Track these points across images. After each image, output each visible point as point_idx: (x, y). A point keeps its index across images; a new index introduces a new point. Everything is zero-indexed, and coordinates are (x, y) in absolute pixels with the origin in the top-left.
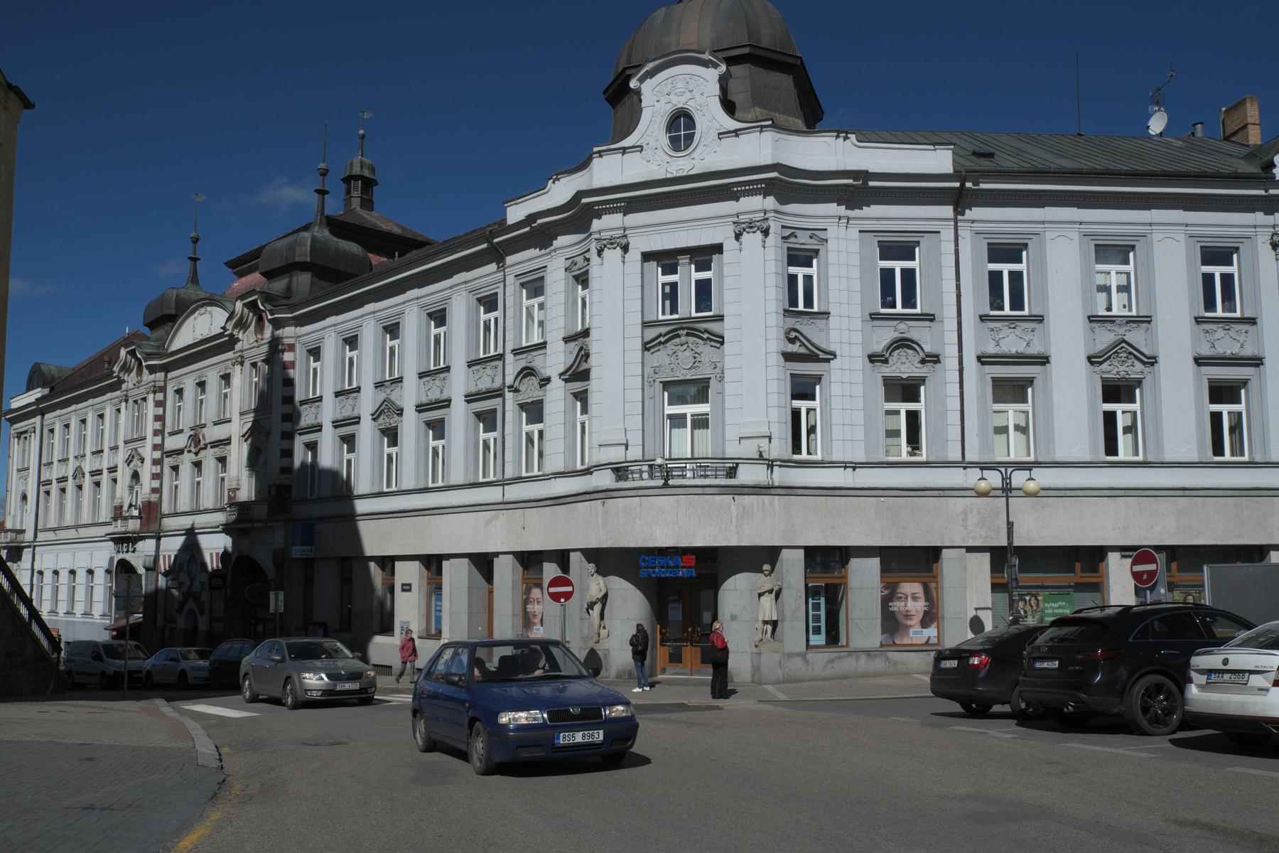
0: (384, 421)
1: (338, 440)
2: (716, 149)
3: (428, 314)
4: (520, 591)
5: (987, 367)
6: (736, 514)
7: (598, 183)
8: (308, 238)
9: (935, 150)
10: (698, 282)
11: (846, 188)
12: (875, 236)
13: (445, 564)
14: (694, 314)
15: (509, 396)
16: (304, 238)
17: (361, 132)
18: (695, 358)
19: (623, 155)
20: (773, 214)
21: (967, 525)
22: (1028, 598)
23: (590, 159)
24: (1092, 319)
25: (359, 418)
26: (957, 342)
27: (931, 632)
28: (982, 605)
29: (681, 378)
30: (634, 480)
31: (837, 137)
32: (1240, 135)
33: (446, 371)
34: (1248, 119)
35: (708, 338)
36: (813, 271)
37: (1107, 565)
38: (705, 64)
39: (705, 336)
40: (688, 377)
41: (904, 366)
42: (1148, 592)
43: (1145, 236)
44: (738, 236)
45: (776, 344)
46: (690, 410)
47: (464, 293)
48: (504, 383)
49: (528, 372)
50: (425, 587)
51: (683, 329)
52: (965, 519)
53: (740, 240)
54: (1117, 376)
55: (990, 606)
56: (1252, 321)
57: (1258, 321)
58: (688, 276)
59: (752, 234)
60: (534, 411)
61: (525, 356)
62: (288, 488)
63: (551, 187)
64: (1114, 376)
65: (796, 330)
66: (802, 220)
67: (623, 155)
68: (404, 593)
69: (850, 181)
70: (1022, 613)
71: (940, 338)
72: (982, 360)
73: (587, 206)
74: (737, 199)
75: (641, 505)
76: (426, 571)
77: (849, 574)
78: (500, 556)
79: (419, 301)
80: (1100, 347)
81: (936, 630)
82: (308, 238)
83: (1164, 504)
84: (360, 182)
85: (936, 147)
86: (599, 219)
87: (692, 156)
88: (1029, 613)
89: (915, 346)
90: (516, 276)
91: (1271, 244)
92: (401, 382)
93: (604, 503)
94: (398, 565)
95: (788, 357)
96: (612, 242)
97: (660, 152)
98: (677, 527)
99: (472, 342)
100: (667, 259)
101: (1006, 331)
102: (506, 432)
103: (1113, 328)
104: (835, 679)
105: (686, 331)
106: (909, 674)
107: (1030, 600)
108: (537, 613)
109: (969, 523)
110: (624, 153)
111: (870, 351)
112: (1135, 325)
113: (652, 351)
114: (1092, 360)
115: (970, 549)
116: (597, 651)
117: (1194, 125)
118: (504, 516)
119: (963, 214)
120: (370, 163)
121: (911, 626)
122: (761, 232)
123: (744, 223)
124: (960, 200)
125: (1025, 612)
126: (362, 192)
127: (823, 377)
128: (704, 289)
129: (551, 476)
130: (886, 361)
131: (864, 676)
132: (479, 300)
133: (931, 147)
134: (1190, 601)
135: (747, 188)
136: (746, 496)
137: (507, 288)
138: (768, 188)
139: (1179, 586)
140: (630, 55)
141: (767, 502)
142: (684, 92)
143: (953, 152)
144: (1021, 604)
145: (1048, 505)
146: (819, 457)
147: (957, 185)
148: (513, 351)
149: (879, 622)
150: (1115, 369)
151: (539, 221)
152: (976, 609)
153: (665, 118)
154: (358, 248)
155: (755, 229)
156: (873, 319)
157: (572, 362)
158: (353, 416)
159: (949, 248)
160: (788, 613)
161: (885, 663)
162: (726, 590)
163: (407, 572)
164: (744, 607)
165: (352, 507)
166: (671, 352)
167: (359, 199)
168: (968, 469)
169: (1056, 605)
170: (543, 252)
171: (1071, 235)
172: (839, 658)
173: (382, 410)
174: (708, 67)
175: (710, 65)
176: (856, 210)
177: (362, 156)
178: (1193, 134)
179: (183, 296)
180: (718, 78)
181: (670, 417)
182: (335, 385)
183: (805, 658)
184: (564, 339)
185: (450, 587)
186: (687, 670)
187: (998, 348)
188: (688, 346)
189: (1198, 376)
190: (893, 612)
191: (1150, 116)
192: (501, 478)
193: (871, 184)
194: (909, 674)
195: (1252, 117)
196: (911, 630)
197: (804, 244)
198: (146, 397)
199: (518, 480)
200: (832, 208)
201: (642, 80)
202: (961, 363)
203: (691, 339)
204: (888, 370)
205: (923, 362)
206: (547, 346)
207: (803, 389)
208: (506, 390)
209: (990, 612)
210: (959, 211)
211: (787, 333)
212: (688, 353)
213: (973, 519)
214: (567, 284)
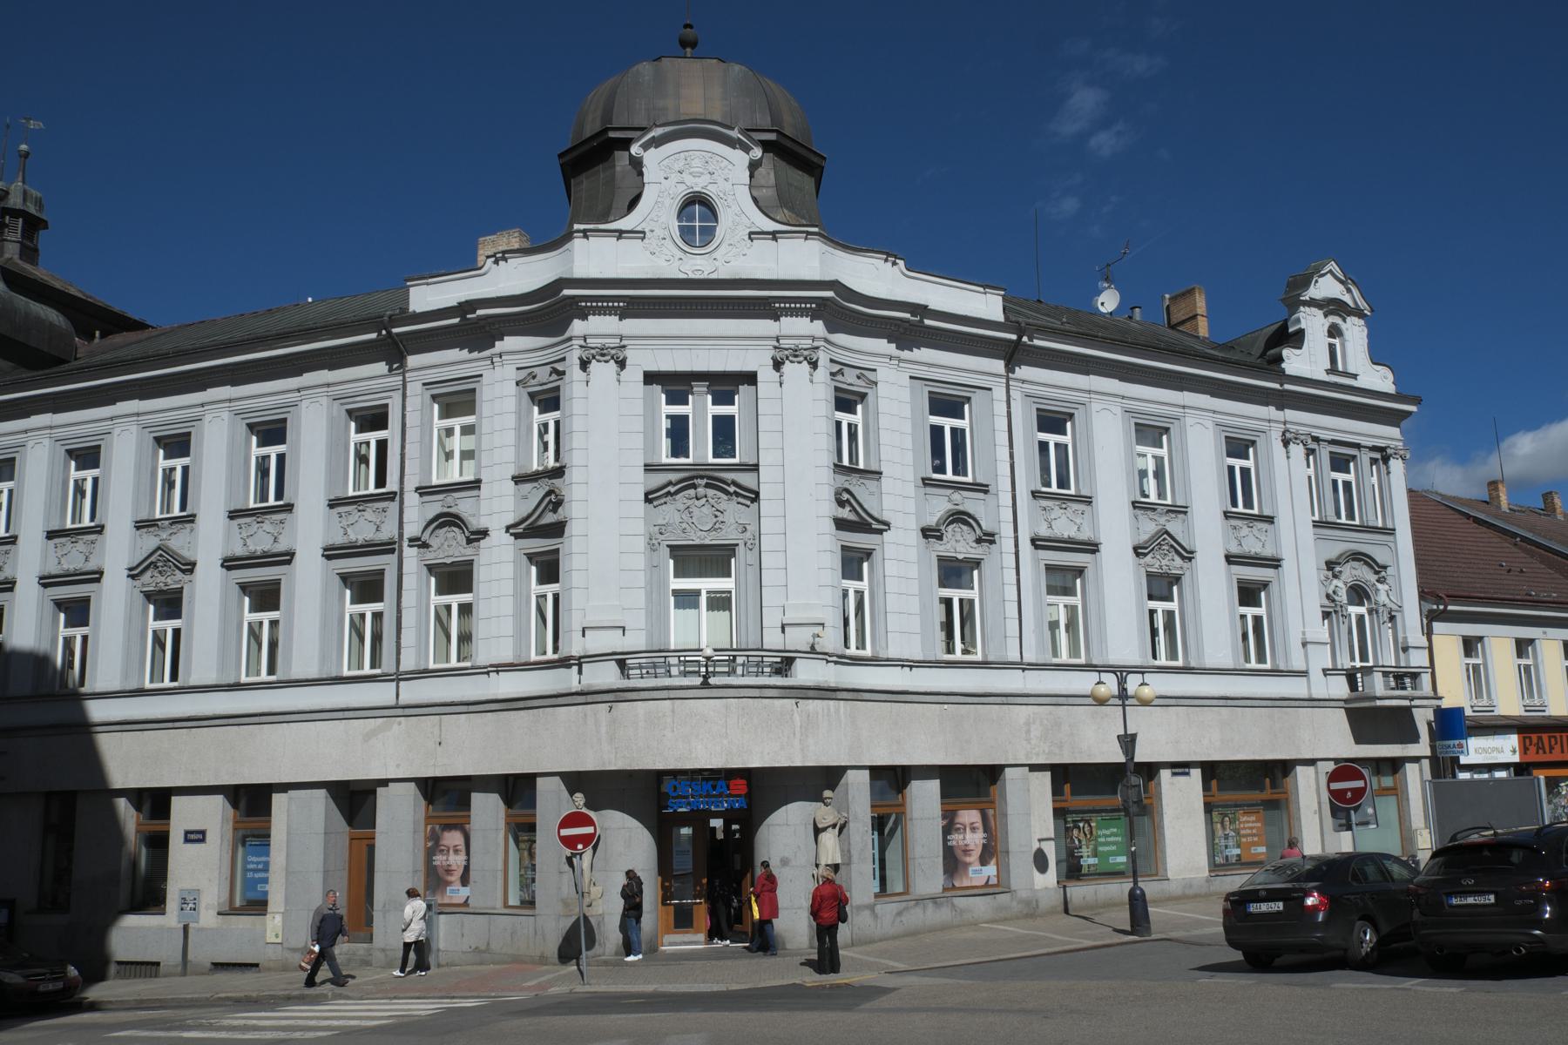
0: (151, 580)
1: (50, 606)
2: (746, 251)
3: (248, 425)
4: (423, 834)
5: (1040, 552)
6: (799, 724)
7: (580, 272)
9: (985, 293)
10: (716, 418)
11: (899, 322)
12: (926, 385)
13: (278, 800)
14: (711, 460)
15: (410, 553)
17: (24, 147)
18: (716, 517)
19: (618, 239)
20: (823, 343)
21: (1031, 739)
22: (1081, 825)
23: (568, 237)
24: (1137, 505)
25: (101, 573)
26: (1012, 520)
27: (991, 870)
28: (1045, 836)
29: (697, 542)
30: (656, 677)
31: (886, 260)
32: (1188, 325)
33: (288, 510)
34: (1198, 310)
35: (735, 492)
36: (857, 418)
37: (1159, 784)
38: (731, 143)
39: (732, 489)
40: (707, 542)
41: (959, 544)
42: (1352, 812)
43: (110, 433)
44: (777, 365)
45: (829, 509)
46: (705, 585)
47: (324, 401)
48: (401, 535)
49: (449, 520)
50: (229, 835)
51: (702, 477)
52: (1028, 732)
53: (588, 370)
54: (1160, 571)
55: (1053, 836)
56: (1270, 520)
57: (1275, 520)
58: (702, 410)
59: (603, 363)
60: (456, 578)
61: (440, 497)
63: (490, 269)
64: (1156, 570)
65: (848, 491)
66: (840, 351)
67: (618, 239)
68: (190, 846)
69: (908, 316)
70: (1077, 842)
71: (993, 512)
72: (1036, 543)
73: (568, 301)
74: (777, 318)
75: (673, 711)
76: (232, 810)
77: (908, 800)
78: (390, 784)
79: (232, 404)
80: (1144, 537)
81: (995, 867)
83: (1210, 715)
84: (21, 220)
85: (987, 290)
86: (583, 320)
87: (714, 255)
88: (1084, 842)
89: (971, 521)
90: (424, 384)
91: (1282, 441)
92: (192, 521)
93: (611, 708)
94: (177, 802)
95: (841, 524)
96: (602, 353)
97: (668, 242)
98: (725, 742)
99: (335, 471)
100: (675, 384)
101: (1057, 512)
102: (404, 604)
103: (1155, 517)
104: (903, 936)
105: (705, 481)
106: (976, 925)
107: (1084, 828)
108: (454, 868)
109: (1032, 736)
110: (619, 238)
111: (924, 524)
112: (1173, 516)
113: (655, 503)
114: (1138, 551)
115: (1034, 768)
116: (590, 918)
117: (1133, 308)
118: (400, 727)
119: (1013, 373)
120: (39, 195)
121: (970, 864)
122: (616, 362)
123: (786, 349)
124: (1013, 355)
125: (1080, 841)
126: (23, 236)
127: (874, 552)
128: (724, 430)
129: (489, 669)
130: (940, 538)
131: (932, 930)
132: (350, 412)
133: (981, 289)
134: (1564, 820)
135: (600, 304)
136: (811, 701)
137: (408, 399)
138: (819, 310)
139: (1218, 806)
140: (607, 114)
141: (832, 709)
142: (702, 174)
143: (1003, 299)
144: (1075, 832)
145: (1106, 715)
146: (868, 652)
147: (1014, 337)
148: (417, 489)
149: (941, 859)
150: (1156, 562)
151: (480, 312)
152: (1040, 840)
153: (678, 200)
154: (57, 316)
155: (608, 358)
156: (925, 485)
157: (530, 510)
158: (84, 570)
159: (1001, 408)
160: (855, 853)
161: (952, 912)
162: (773, 825)
163: (212, 814)
164: (799, 847)
165: (82, 712)
166: (682, 507)
167: (18, 245)
168: (1026, 672)
169: (1108, 832)
170: (475, 355)
171: (1113, 408)
172: (906, 909)
173: (152, 563)
174: (734, 148)
175: (738, 146)
176: (906, 351)
177: (24, 182)
178: (1130, 318)
180: (747, 164)
181: (676, 593)
182: (47, 518)
183: (874, 911)
184: (513, 478)
185: (289, 833)
186: (701, 937)
187: (345, 537)
188: (707, 501)
189: (1230, 575)
190: (952, 847)
191: (1099, 293)
192: (393, 670)
193: (927, 322)
194: (976, 925)
195: (1200, 308)
196: (970, 869)
197: (852, 385)
199: (425, 673)
200: (882, 345)
201: (646, 147)
202: (1016, 546)
203: (711, 492)
204: (942, 548)
205: (979, 541)
206: (482, 485)
207: (853, 563)
208: (406, 543)
209: (1053, 843)
210: (1010, 368)
211: (838, 494)
212: (707, 510)
213: (1036, 732)
214: (519, 403)
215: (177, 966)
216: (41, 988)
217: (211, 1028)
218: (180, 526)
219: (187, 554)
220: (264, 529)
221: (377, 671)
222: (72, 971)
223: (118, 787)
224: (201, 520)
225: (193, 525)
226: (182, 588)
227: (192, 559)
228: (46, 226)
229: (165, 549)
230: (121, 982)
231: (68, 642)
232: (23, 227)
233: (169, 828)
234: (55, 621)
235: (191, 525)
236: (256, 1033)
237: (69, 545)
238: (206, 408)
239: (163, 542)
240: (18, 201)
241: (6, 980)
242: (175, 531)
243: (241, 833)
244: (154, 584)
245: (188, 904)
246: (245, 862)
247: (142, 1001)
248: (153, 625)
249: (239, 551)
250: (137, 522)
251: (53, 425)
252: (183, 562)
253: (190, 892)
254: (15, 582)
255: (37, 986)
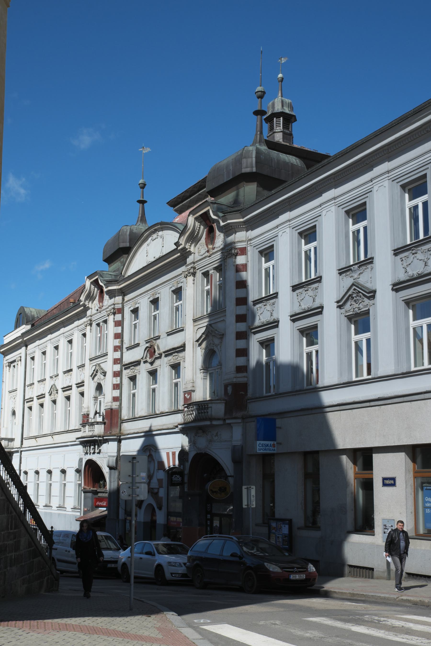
8: (252, 150)
16: (250, 151)
17: (280, 75)
43: (320, 215)
62: (244, 386)
68: (386, 488)
76: (412, 463)
82: (252, 150)
84: (281, 118)
94: (377, 458)
120: (290, 101)
126: (283, 128)
165: (319, 399)
173: (350, 295)
179: (135, 231)
198: (107, 320)
215: (383, 572)
216: (292, 577)
217: (378, 625)
218: (364, 267)
219: (369, 286)
220: (417, 258)
221: (370, 377)
222: (312, 568)
223: (340, 448)
224: (377, 261)
225: (373, 265)
226: (369, 310)
227: (374, 289)
228: (295, 120)
229: (356, 284)
230: (353, 579)
231: (309, 355)
232: (283, 122)
233: (373, 476)
234: (301, 342)
235: (371, 265)
236: (407, 636)
237: (304, 293)
238: (374, 182)
239: (355, 280)
240: (279, 107)
241: (271, 570)
242: (361, 271)
243: (420, 480)
244: (352, 310)
245: (388, 529)
246: (424, 502)
247: (353, 595)
248: (354, 338)
249: (402, 277)
250: (339, 270)
251: (290, 219)
252: (368, 291)
253: (389, 520)
254: (279, 321)
255: (289, 576)
